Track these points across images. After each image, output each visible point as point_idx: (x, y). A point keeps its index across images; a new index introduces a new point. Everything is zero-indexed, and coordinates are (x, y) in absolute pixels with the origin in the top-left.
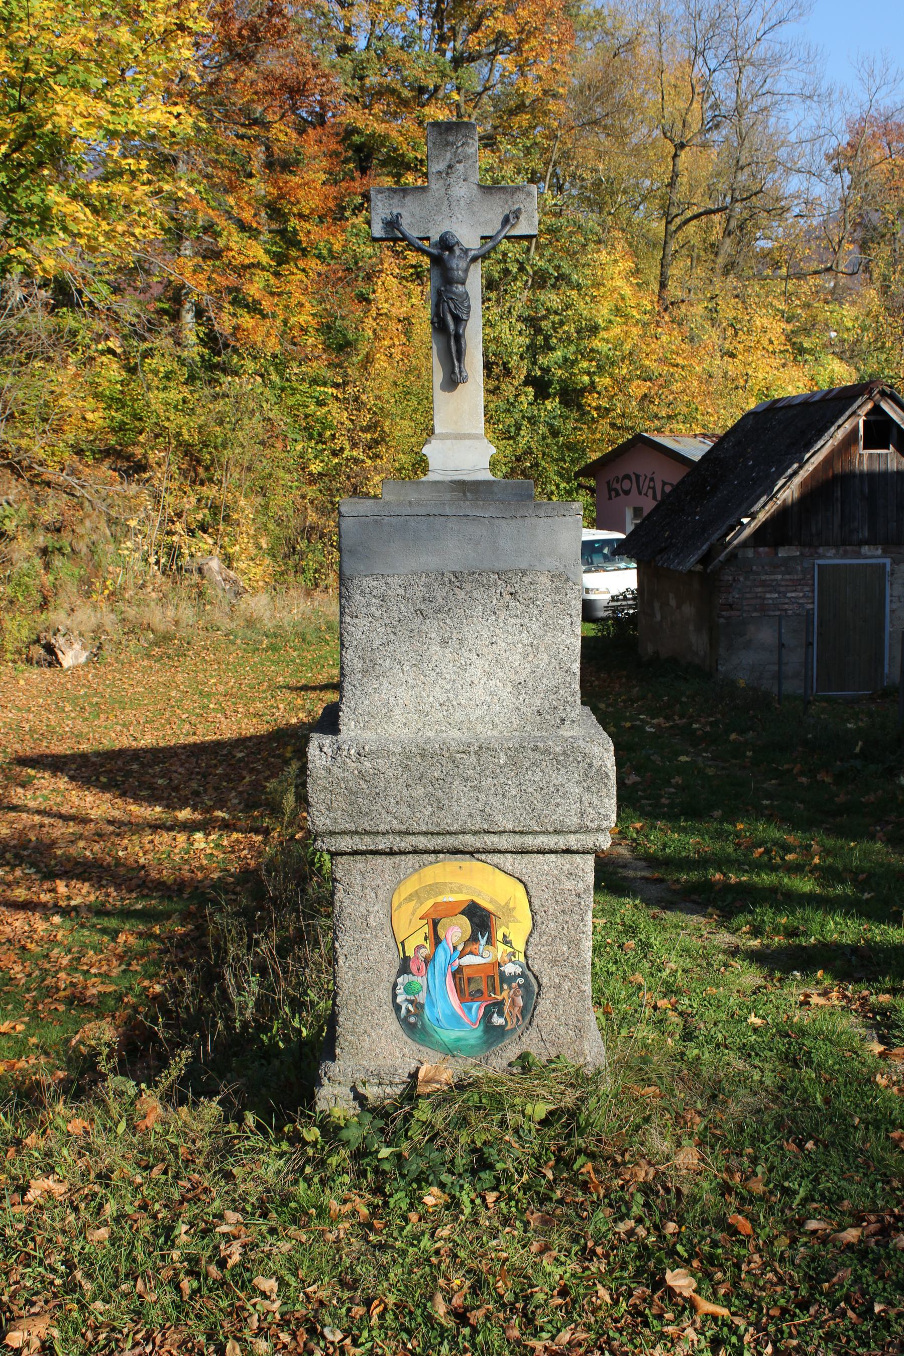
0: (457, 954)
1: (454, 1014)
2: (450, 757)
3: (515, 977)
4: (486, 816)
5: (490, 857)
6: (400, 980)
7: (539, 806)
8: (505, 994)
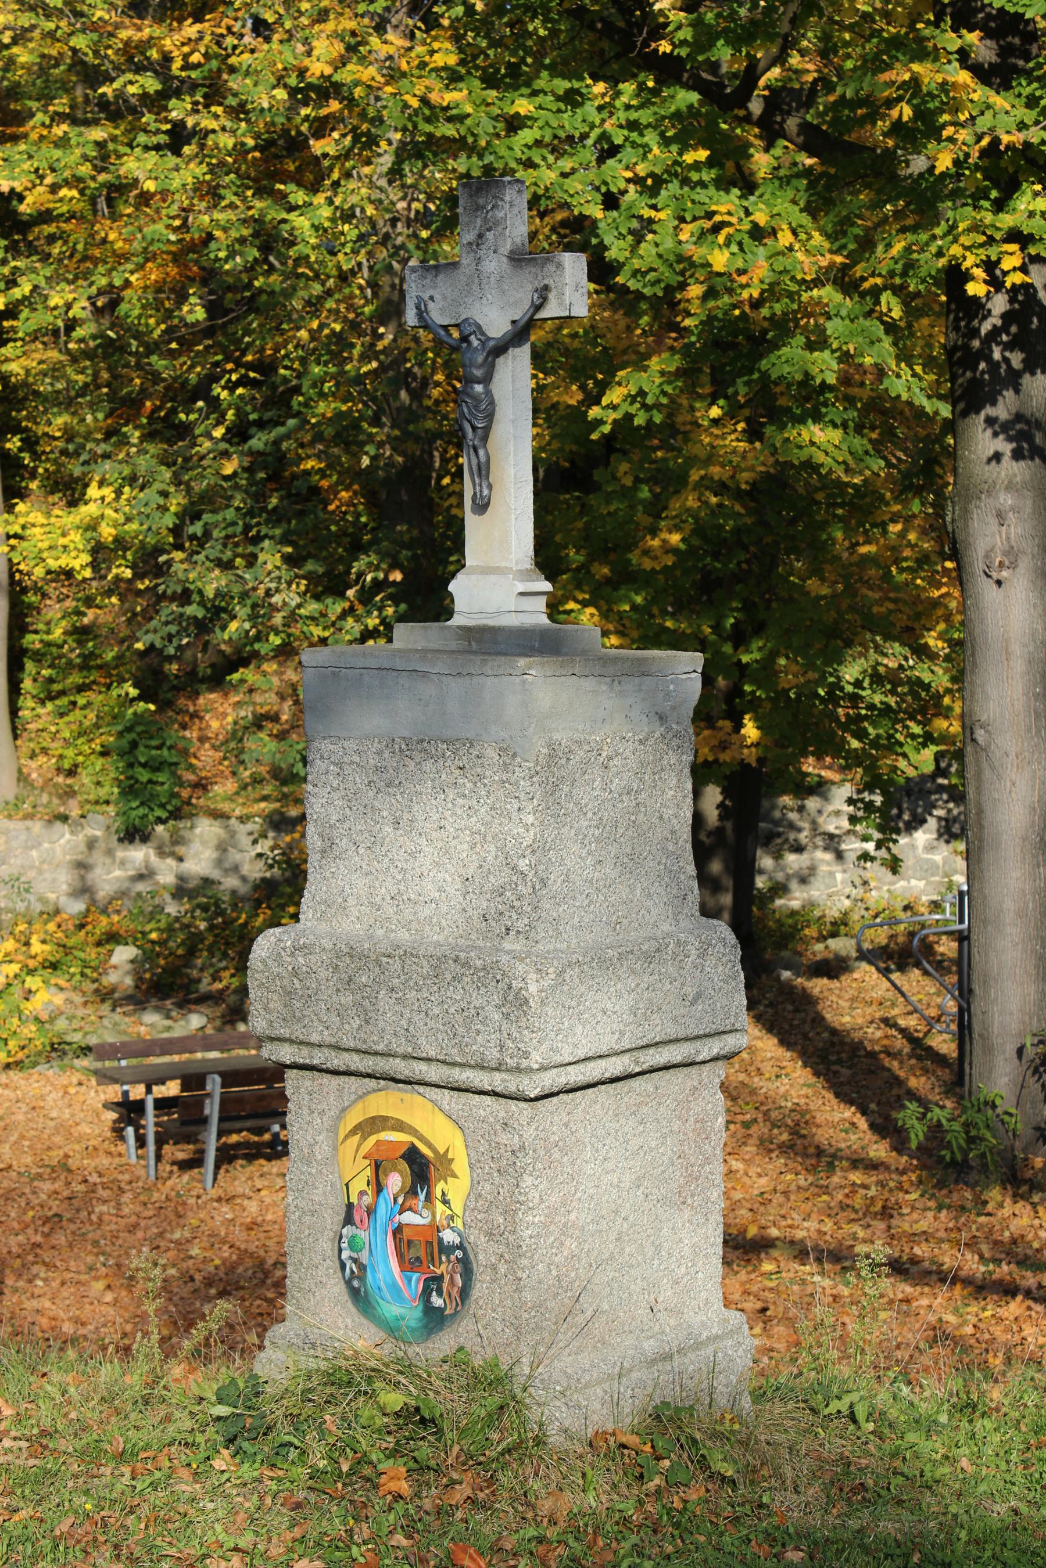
0: (397, 1208)
1: (394, 1284)
2: (377, 960)
3: (453, 1248)
4: (411, 1038)
5: (421, 1089)
6: (344, 1231)
7: (461, 1031)
8: (443, 1267)
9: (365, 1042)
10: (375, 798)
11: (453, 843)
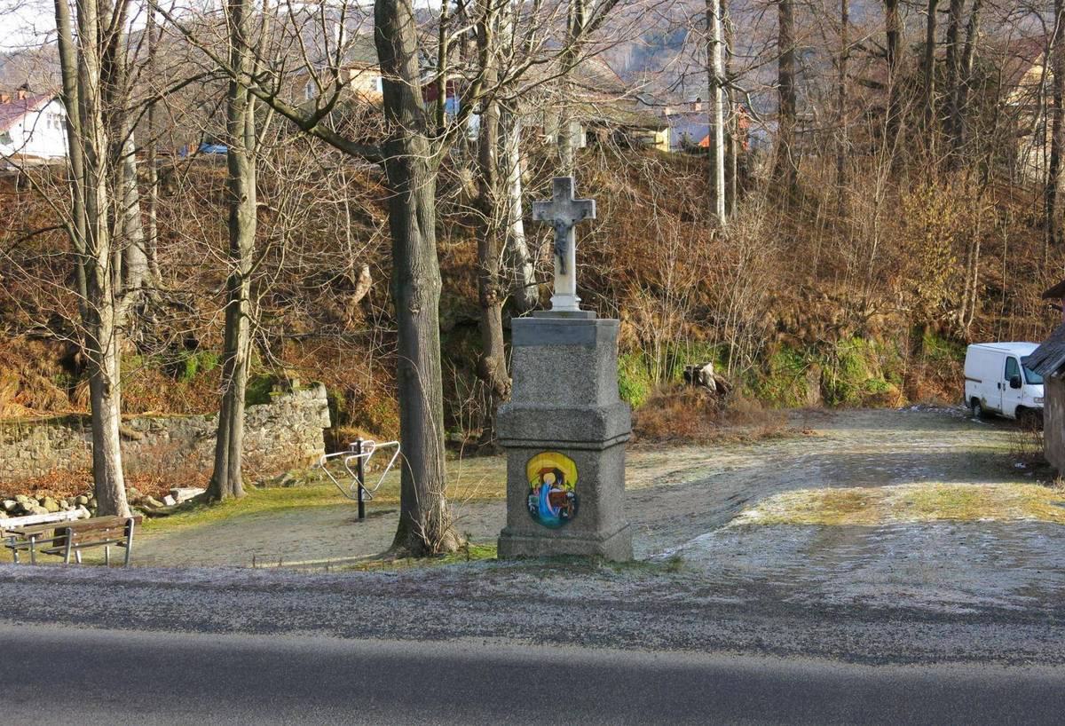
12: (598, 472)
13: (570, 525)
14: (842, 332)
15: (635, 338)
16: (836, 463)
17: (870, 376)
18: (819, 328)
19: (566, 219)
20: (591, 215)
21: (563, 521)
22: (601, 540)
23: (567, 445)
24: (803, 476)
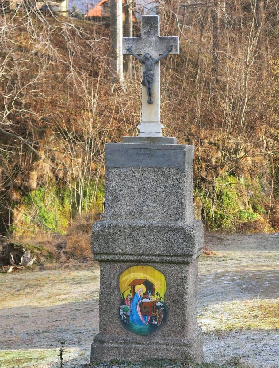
3: (160, 307)
6: (121, 307)
8: (157, 313)
9: (135, 252)
10: (132, 184)
11: (160, 196)
12: (186, 283)
13: (159, 333)
14: (220, 171)
15: (50, 174)
16: (243, 278)
17: (242, 208)
18: (201, 167)
19: (154, 54)
20: (176, 50)
21: (153, 328)
22: (189, 345)
23: (158, 259)
24: (221, 290)
